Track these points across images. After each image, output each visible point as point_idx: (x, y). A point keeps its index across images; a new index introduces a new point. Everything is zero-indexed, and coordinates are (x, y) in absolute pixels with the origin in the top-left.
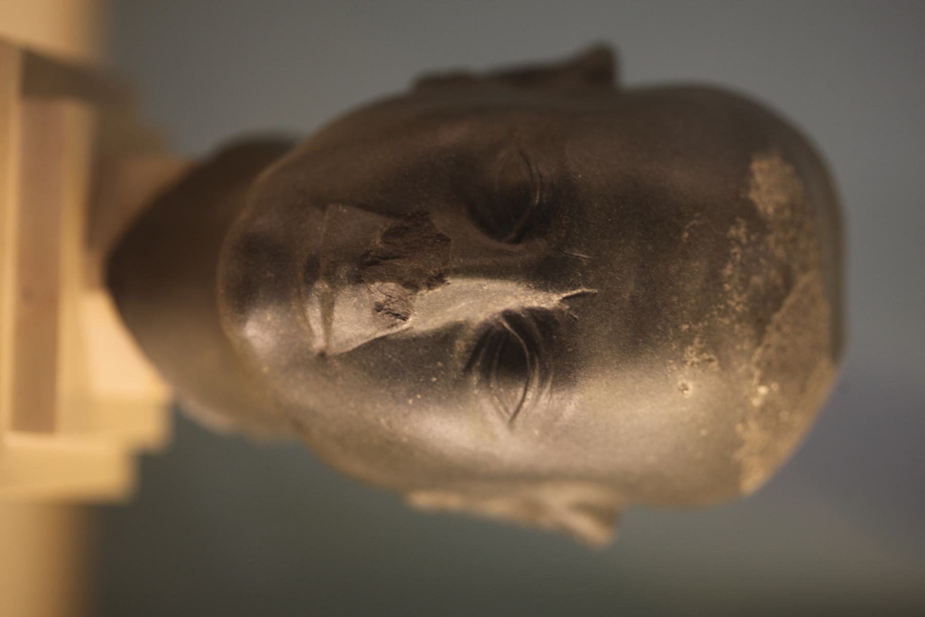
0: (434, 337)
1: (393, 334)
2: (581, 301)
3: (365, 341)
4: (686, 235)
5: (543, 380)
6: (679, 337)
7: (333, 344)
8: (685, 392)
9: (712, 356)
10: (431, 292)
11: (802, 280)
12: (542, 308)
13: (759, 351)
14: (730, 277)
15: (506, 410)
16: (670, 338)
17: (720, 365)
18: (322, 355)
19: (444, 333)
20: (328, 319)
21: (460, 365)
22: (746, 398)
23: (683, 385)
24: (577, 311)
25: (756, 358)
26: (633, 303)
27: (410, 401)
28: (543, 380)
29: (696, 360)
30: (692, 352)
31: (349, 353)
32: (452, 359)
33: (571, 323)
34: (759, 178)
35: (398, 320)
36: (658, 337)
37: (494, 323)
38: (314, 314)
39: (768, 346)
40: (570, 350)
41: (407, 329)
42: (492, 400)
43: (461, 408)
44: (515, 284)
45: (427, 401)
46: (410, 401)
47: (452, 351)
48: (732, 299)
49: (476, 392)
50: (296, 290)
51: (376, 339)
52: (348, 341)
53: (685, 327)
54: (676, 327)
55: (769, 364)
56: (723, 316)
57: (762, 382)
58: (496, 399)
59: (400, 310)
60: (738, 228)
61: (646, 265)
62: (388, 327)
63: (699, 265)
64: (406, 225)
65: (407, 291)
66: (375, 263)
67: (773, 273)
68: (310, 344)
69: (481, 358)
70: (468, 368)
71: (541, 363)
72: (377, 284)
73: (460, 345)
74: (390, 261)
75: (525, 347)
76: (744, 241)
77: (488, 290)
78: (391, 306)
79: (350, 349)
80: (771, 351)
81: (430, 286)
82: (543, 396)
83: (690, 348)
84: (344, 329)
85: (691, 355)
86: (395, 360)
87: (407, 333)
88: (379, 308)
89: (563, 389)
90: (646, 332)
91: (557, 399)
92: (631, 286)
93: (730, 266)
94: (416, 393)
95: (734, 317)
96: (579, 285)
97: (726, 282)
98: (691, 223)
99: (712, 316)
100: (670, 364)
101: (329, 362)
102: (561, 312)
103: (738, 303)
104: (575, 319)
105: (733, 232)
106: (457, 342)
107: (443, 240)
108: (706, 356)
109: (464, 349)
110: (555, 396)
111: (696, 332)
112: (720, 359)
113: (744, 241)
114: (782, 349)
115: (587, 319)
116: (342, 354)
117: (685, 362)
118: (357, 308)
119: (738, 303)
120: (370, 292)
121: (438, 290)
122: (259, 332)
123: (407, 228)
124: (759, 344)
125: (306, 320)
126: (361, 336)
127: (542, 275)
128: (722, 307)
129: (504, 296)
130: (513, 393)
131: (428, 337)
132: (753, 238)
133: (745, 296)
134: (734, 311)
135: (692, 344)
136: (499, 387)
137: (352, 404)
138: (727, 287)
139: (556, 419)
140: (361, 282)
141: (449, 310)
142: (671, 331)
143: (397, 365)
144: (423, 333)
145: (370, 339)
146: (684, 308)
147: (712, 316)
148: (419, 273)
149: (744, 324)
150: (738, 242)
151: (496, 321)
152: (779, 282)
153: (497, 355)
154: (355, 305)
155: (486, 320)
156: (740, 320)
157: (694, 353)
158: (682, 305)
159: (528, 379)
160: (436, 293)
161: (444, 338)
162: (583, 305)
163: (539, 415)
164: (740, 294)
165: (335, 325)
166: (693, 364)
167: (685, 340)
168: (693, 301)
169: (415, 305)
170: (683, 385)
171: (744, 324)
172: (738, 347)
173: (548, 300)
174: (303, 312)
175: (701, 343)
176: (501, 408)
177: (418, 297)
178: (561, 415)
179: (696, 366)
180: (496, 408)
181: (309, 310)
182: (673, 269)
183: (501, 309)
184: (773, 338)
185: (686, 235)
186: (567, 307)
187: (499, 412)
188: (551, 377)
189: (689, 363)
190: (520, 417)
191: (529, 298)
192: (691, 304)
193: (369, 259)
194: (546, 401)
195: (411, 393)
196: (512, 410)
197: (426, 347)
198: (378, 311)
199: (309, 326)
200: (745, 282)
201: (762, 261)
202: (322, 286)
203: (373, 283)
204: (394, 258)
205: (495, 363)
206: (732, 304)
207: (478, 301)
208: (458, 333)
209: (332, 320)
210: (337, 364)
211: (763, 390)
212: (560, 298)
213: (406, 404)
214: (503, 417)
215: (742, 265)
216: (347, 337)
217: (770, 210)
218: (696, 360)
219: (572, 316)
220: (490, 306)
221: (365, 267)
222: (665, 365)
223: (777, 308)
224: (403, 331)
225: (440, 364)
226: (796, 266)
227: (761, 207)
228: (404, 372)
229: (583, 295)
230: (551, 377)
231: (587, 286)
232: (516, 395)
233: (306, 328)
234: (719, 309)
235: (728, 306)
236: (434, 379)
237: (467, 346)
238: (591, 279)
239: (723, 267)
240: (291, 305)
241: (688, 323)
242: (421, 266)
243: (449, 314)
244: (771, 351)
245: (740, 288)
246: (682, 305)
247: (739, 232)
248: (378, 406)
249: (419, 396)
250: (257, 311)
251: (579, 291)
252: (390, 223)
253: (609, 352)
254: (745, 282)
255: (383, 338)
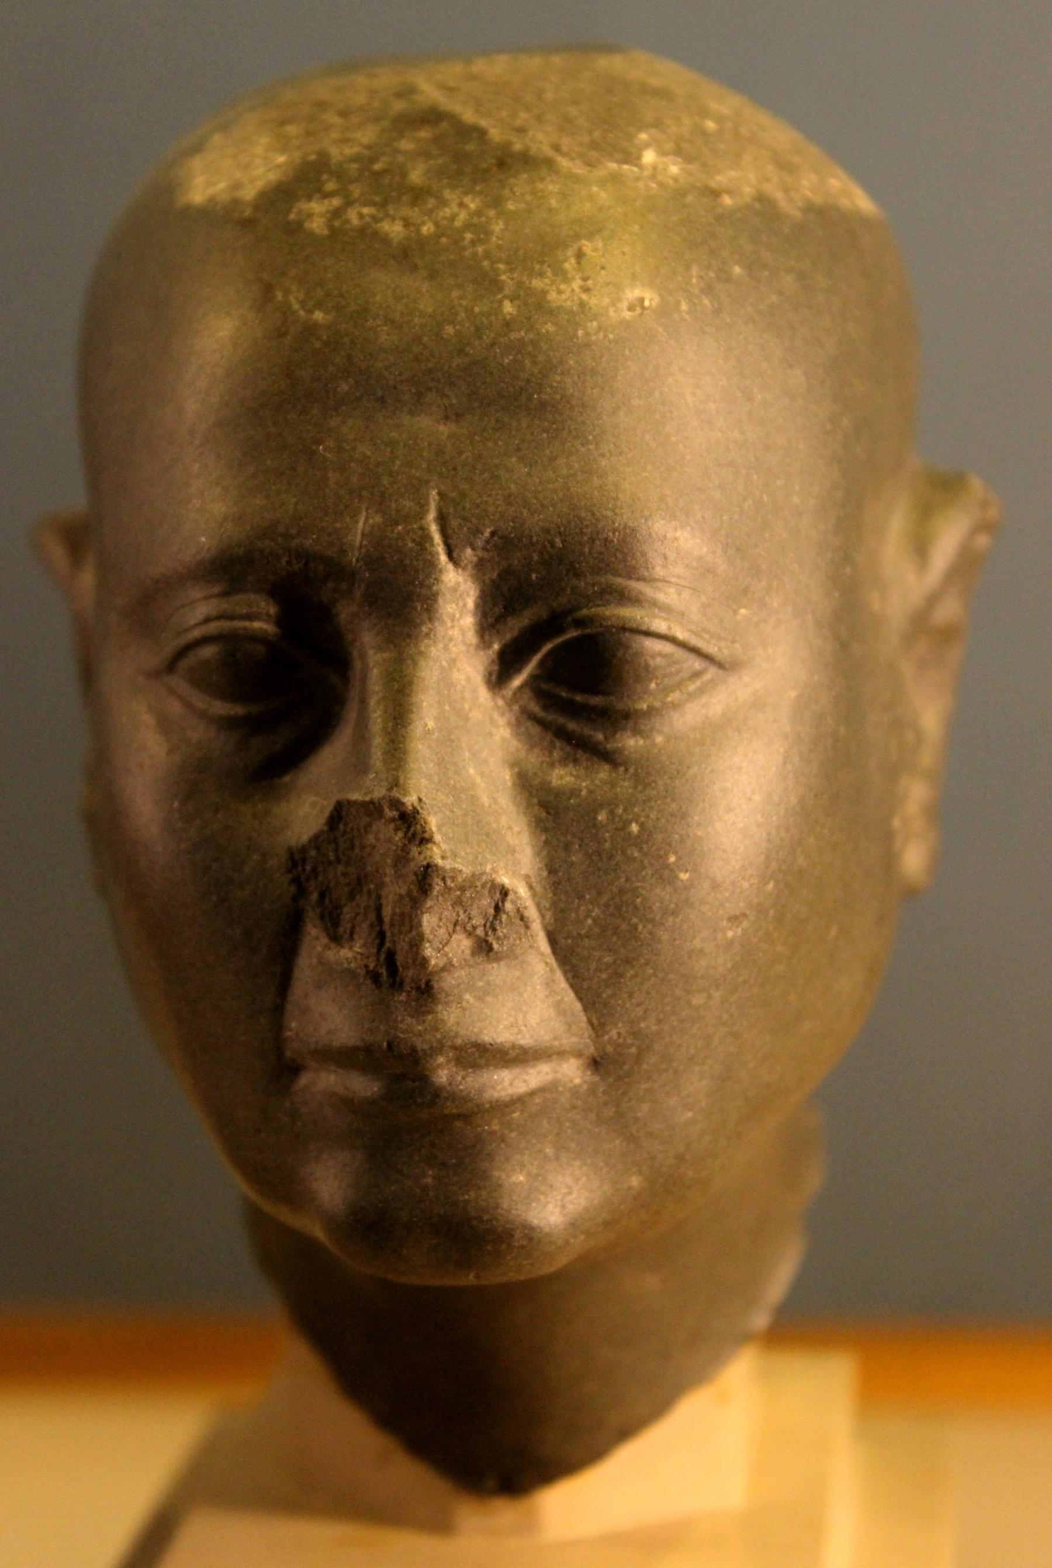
0: (545, 830)
1: (543, 916)
2: (454, 523)
3: (559, 975)
4: (318, 316)
5: (624, 597)
6: (529, 318)
7: (568, 1041)
8: (647, 303)
9: (570, 252)
10: (437, 838)
11: (429, 92)
12: (477, 606)
13: (564, 163)
14: (407, 223)
15: (697, 675)
16: (531, 336)
17: (590, 237)
18: (595, 1064)
19: (536, 809)
20: (513, 1054)
21: (604, 772)
22: (661, 185)
23: (631, 308)
24: (478, 531)
25: (578, 169)
26: (458, 416)
27: (684, 876)
28: (624, 597)
29: (576, 284)
30: (559, 292)
31: (586, 1009)
32: (590, 792)
33: (504, 543)
34: (220, 187)
35: (508, 906)
36: (527, 362)
37: (516, 708)
38: (505, 1083)
39: (557, 148)
40: (558, 542)
41: (531, 888)
42: (676, 706)
43: (695, 769)
44: (422, 663)
45: (682, 841)
46: (684, 876)
47: (574, 792)
48: (453, 218)
49: (659, 739)
50: (458, 1124)
51: (555, 952)
52: (559, 1008)
53: (508, 308)
54: (507, 324)
55: (594, 145)
56: (488, 233)
57: (631, 157)
58: (674, 697)
59: (486, 902)
60: (310, 215)
61: (380, 393)
62: (527, 927)
63: (383, 286)
64: (315, 896)
65: (438, 887)
66: (390, 959)
67: (406, 145)
68: (575, 1091)
69: (587, 731)
70: (609, 757)
71: (589, 601)
72: (428, 951)
73: (562, 777)
74: (386, 927)
75: (559, 640)
76: (336, 202)
77: (437, 719)
78: (478, 921)
79: (578, 1006)
80: (566, 142)
81: (425, 840)
82: (661, 597)
83: (553, 296)
84: (533, 1020)
85: (564, 294)
86: (596, 912)
87: (538, 888)
88: (484, 948)
89: (644, 554)
90: (516, 387)
91: (665, 566)
92: (424, 422)
93: (385, 226)
94: (667, 866)
95: (492, 213)
96: (422, 528)
97: (418, 230)
98: (296, 306)
99: (487, 255)
100: (587, 334)
101: (609, 1049)
102: (480, 566)
103: (461, 205)
104: (493, 534)
105: (317, 226)
106: (555, 782)
107: (340, 818)
108: (570, 265)
109: (570, 768)
110: (659, 572)
111: (520, 284)
112: (577, 237)
113: (336, 202)
114: (566, 124)
115: (491, 509)
116: (590, 1022)
117: (582, 304)
118: (487, 993)
119: (460, 207)
120: (448, 967)
121: (433, 822)
122: (552, 1196)
123: (322, 896)
124: (549, 163)
125: (519, 1101)
126: (549, 983)
127: (401, 602)
128: (468, 236)
129: (451, 685)
130: (659, 660)
131: (546, 842)
132: (331, 186)
133: (447, 194)
134: (478, 213)
135: (544, 293)
136: (646, 691)
137: (698, 1000)
138: (427, 229)
139: (710, 571)
140: (429, 986)
141: (485, 800)
142: (514, 336)
143: (607, 905)
144: (538, 854)
145: (555, 965)
146: (469, 311)
147: (487, 255)
148: (402, 858)
149: (506, 192)
150: (336, 213)
151: (509, 704)
152: (425, 134)
153: (579, 698)
154: (480, 999)
155: (509, 724)
156: (497, 202)
157: (562, 287)
158: (462, 315)
159: (624, 629)
160: (439, 827)
161: (552, 814)
162: (464, 518)
163: (704, 607)
164: (444, 203)
165: (525, 1040)
166: (586, 290)
167: (536, 306)
168: (455, 294)
169: (467, 871)
170: (631, 308)
171: (506, 192)
172: (553, 202)
173: (457, 596)
174: (501, 1107)
175: (541, 274)
176: (692, 687)
177: (447, 864)
178: (700, 558)
179: (590, 282)
180: (691, 697)
181: (496, 1095)
182: (386, 337)
183: (484, 694)
184: (540, 140)
185: (318, 316)
186: (469, 551)
187: (701, 691)
188: (620, 581)
189: (584, 297)
190: (710, 648)
191: (455, 633)
192: (461, 297)
193: (383, 971)
194: (672, 590)
195: (665, 876)
196: (697, 664)
197: (567, 847)
198: (490, 948)
199: (532, 1093)
200: (418, 195)
201: (377, 167)
202: (443, 1074)
203: (425, 961)
204: (380, 919)
205: (596, 700)
206: (463, 215)
207: (458, 734)
208: (537, 782)
209: (514, 1046)
210: (614, 1033)
211: (649, 157)
212: (450, 566)
213: (689, 886)
214: (713, 683)
215: (384, 204)
216: (552, 1012)
217: (281, 159)
218: (576, 284)
219: (487, 542)
220: (476, 715)
221: (399, 977)
222: (587, 345)
223: (482, 133)
224: (534, 895)
225: (602, 817)
226: (399, 106)
227: (273, 177)
228: (621, 892)
229: (442, 520)
230: (620, 581)
231: (421, 515)
232: (661, 655)
233: (537, 1100)
234: (473, 242)
235: (468, 226)
236: (634, 828)
237: (564, 761)
238: (408, 504)
239: (385, 240)
240: (492, 1133)
241: (500, 302)
242: (389, 861)
243: (495, 802)
244: (566, 142)
245: (431, 202)
246: (462, 315)
247: (315, 214)
248: (697, 943)
249: (672, 859)
250: (505, 1203)
251: (434, 529)
252: (313, 934)
253: (562, 461)
254: (418, 195)
255: (552, 939)
